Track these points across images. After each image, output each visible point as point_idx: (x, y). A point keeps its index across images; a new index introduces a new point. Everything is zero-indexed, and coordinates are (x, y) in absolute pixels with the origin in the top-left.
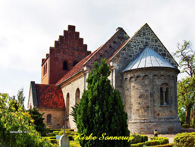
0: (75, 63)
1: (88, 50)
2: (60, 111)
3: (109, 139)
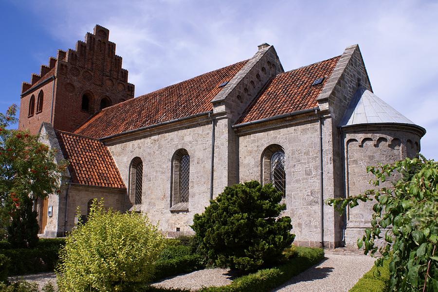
0: (105, 102)
1: (128, 82)
2: (113, 195)
3: (271, 269)
